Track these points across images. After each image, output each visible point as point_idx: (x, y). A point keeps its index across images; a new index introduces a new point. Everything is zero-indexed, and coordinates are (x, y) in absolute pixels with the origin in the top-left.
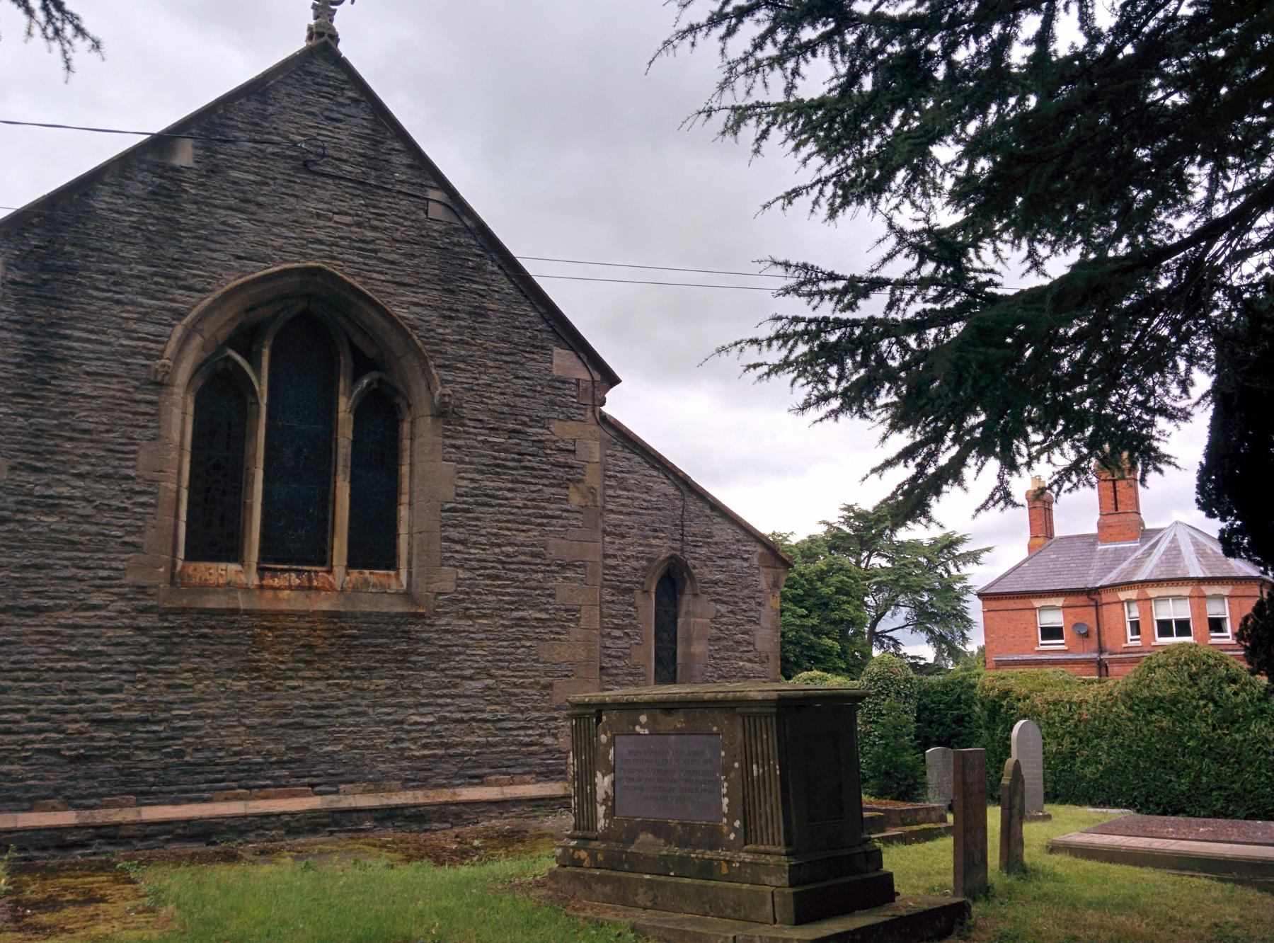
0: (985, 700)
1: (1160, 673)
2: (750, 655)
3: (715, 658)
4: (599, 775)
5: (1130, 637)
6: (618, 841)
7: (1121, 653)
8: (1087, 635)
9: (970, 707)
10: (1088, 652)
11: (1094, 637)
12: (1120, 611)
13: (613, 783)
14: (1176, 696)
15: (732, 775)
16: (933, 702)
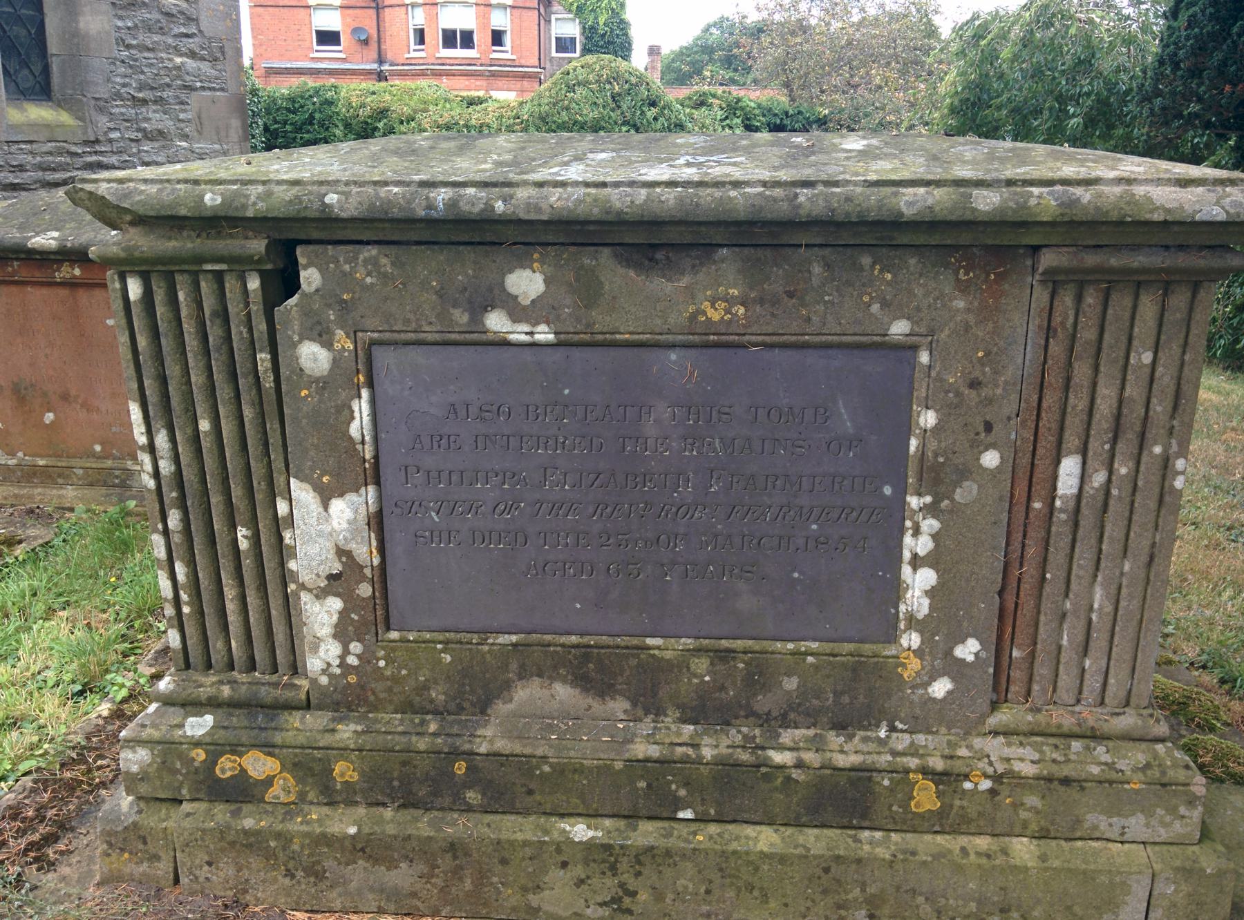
0: (354, 122)
1: (581, 92)
2: (193, 43)
3: (128, 47)
4: (302, 493)
5: (412, 46)
6: (407, 707)
7: (403, 65)
8: (366, 42)
9: (327, 129)
10: (367, 62)
11: (374, 45)
12: (404, 16)
13: (377, 522)
14: (597, 120)
15: (965, 493)
16: (276, 122)
